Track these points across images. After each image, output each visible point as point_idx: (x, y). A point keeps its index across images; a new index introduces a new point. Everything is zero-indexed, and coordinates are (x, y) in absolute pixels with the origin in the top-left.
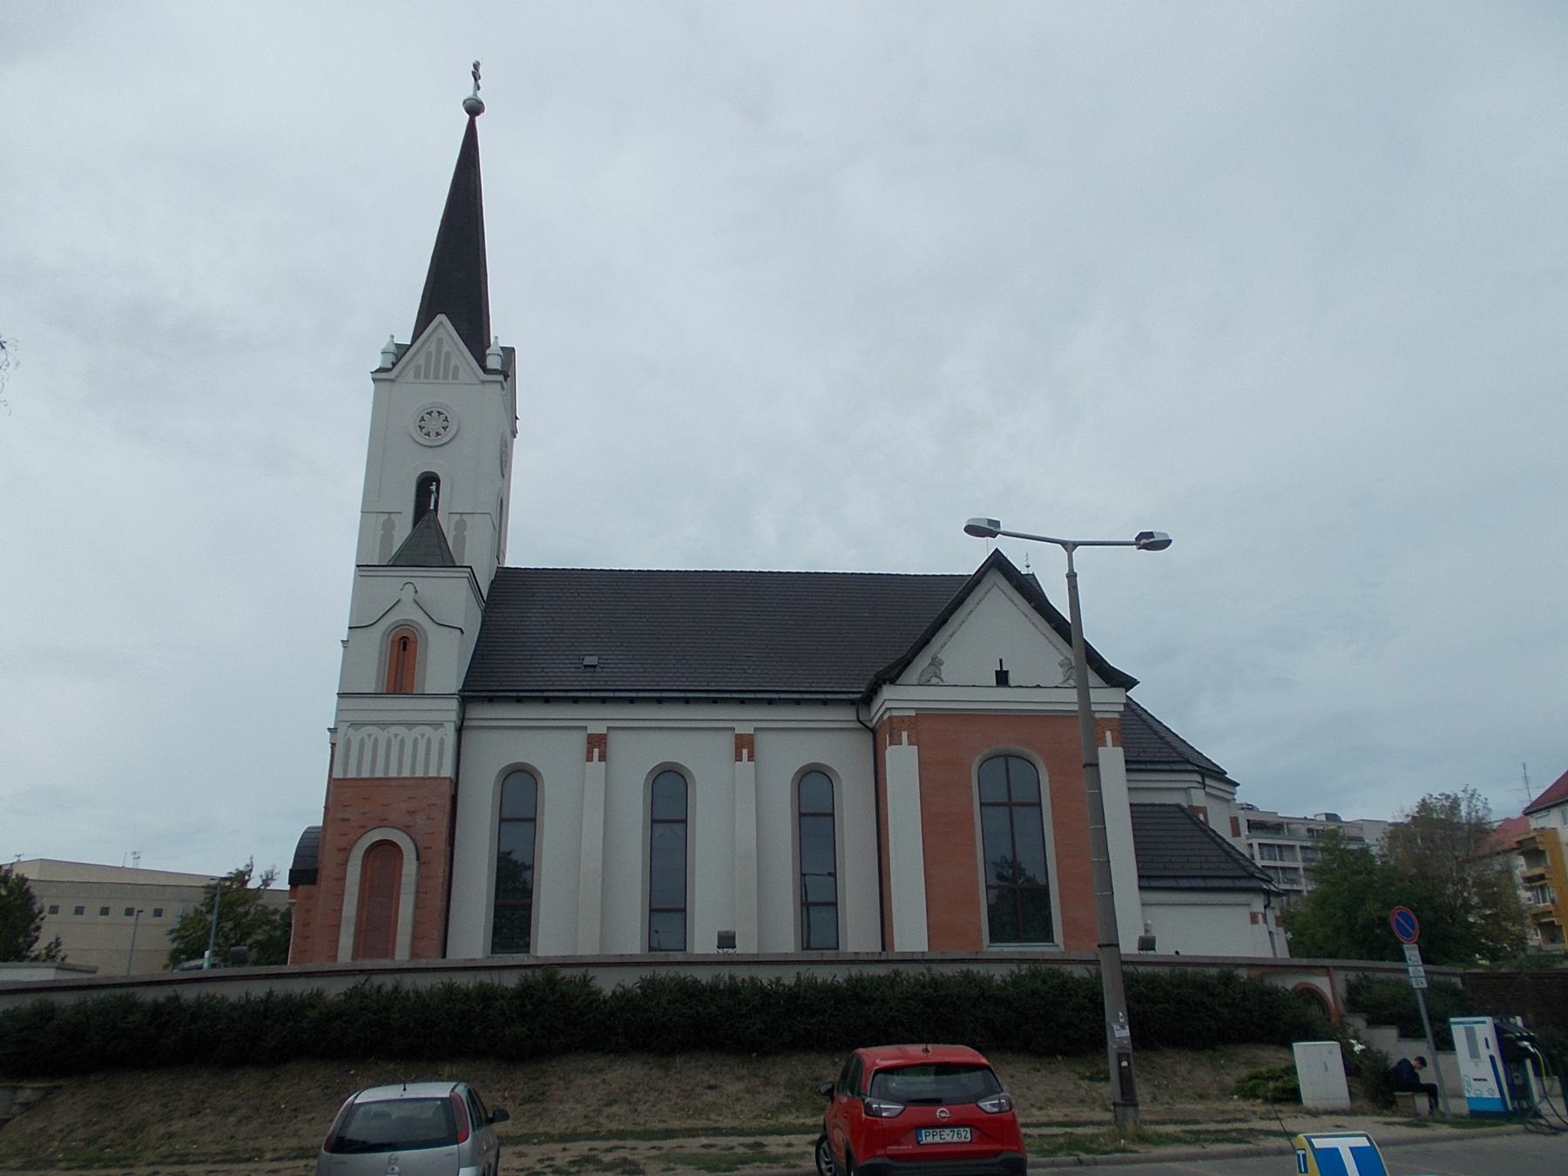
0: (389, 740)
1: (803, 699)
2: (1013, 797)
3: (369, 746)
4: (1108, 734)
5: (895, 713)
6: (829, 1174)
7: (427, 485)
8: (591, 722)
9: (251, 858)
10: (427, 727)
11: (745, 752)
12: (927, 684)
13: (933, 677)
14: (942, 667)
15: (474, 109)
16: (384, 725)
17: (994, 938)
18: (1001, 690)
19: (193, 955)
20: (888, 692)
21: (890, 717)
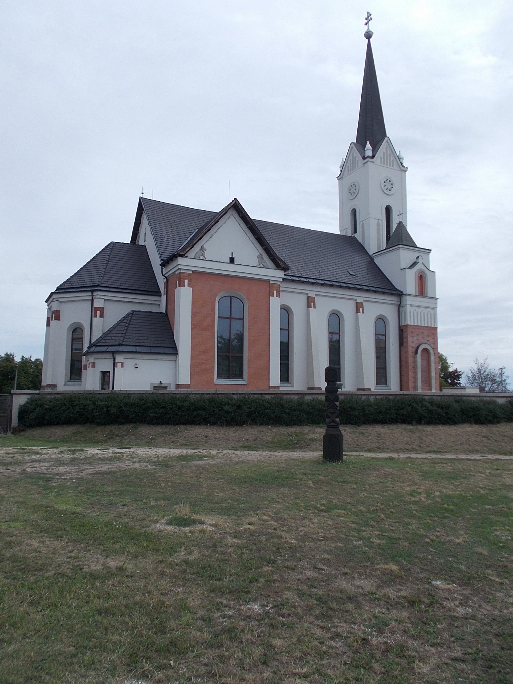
1: (325, 284)
2: (240, 317)
3: (422, 313)
5: (182, 271)
7: (354, 212)
9: (232, 253)
10: (430, 309)
14: (205, 252)
15: (368, 36)
16: (419, 307)
18: (232, 265)
20: (181, 261)
21: (180, 273)
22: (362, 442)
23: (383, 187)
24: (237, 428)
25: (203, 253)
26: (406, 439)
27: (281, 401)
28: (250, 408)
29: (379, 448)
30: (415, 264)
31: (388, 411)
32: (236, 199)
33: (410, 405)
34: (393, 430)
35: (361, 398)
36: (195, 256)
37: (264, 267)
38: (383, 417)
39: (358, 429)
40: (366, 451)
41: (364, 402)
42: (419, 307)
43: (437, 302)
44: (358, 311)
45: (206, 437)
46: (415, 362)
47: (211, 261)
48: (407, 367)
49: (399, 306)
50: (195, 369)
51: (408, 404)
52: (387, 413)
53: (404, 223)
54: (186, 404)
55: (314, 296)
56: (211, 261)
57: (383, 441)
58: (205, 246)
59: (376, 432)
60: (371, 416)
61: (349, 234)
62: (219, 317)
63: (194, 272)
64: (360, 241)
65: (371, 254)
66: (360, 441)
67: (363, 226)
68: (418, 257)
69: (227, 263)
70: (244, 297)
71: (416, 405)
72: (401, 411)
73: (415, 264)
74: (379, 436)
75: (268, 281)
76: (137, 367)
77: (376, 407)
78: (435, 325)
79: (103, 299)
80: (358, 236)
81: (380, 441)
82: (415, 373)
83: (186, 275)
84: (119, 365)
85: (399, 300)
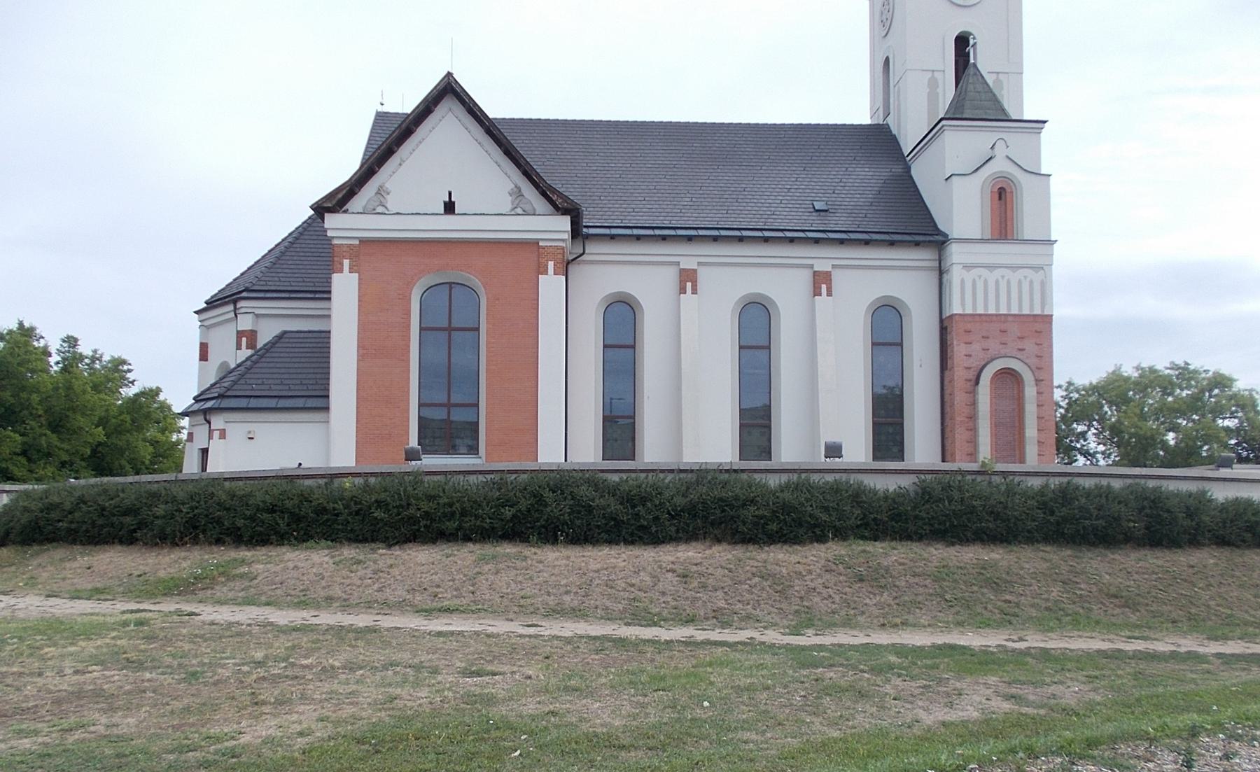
0: (974, 281)
1: (851, 240)
4: (551, 264)
8: (818, 260)
9: (450, 194)
10: (1030, 271)
11: (689, 285)
14: (388, 197)
16: (991, 267)
18: (450, 217)
25: (382, 199)
32: (449, 74)
36: (365, 208)
37: (526, 213)
42: (991, 267)
44: (817, 292)
45: (89, 568)
46: (974, 404)
47: (398, 213)
49: (941, 272)
55: (695, 267)
56: (398, 213)
58: (387, 185)
62: (478, 329)
63: (364, 241)
64: (894, 131)
69: (358, 213)
70: (476, 282)
75: (535, 243)
76: (252, 438)
78: (1043, 307)
79: (251, 315)
82: (974, 430)
83: (344, 249)
84: (216, 434)
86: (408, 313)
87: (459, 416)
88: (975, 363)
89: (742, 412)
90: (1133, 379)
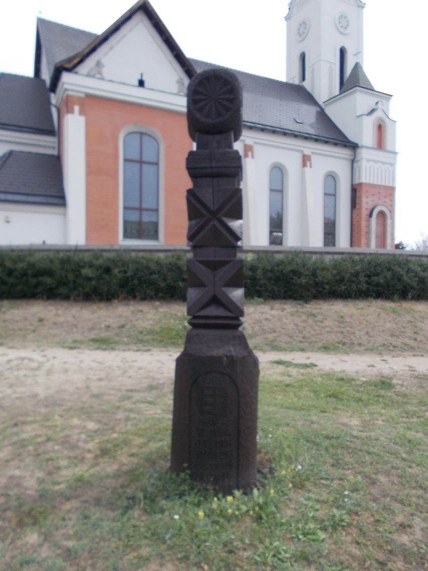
6: (426, 565)
7: (303, 57)
9: (142, 75)
12: (93, 76)
13: (97, 72)
16: (376, 162)
17: (127, 235)
18: (141, 90)
19: (63, 290)
22: (313, 332)
23: (339, 27)
24: (102, 305)
26: (388, 325)
27: (178, 262)
28: (125, 272)
29: (344, 344)
30: (373, 111)
31: (354, 279)
33: (389, 269)
34: (362, 308)
35: (311, 258)
38: (346, 287)
39: (306, 307)
40: (319, 348)
41: (315, 263)
42: (376, 162)
43: (395, 159)
44: (304, 165)
46: (369, 226)
48: (359, 233)
49: (353, 161)
50: (93, 224)
51: (386, 267)
52: (353, 282)
53: (361, 63)
54: (20, 266)
57: (348, 329)
59: (336, 312)
60: (327, 287)
61: (296, 81)
63: (89, 97)
65: (321, 103)
66: (309, 329)
67: (313, 71)
68: (377, 103)
70: (158, 134)
71: (399, 269)
72: (375, 279)
73: (373, 111)
74: (340, 320)
77: (335, 272)
80: (307, 85)
81: (344, 330)
85: (353, 154)
86: (116, 148)
87: (147, 218)
88: (370, 207)
89: (325, 218)
90: (235, 224)
